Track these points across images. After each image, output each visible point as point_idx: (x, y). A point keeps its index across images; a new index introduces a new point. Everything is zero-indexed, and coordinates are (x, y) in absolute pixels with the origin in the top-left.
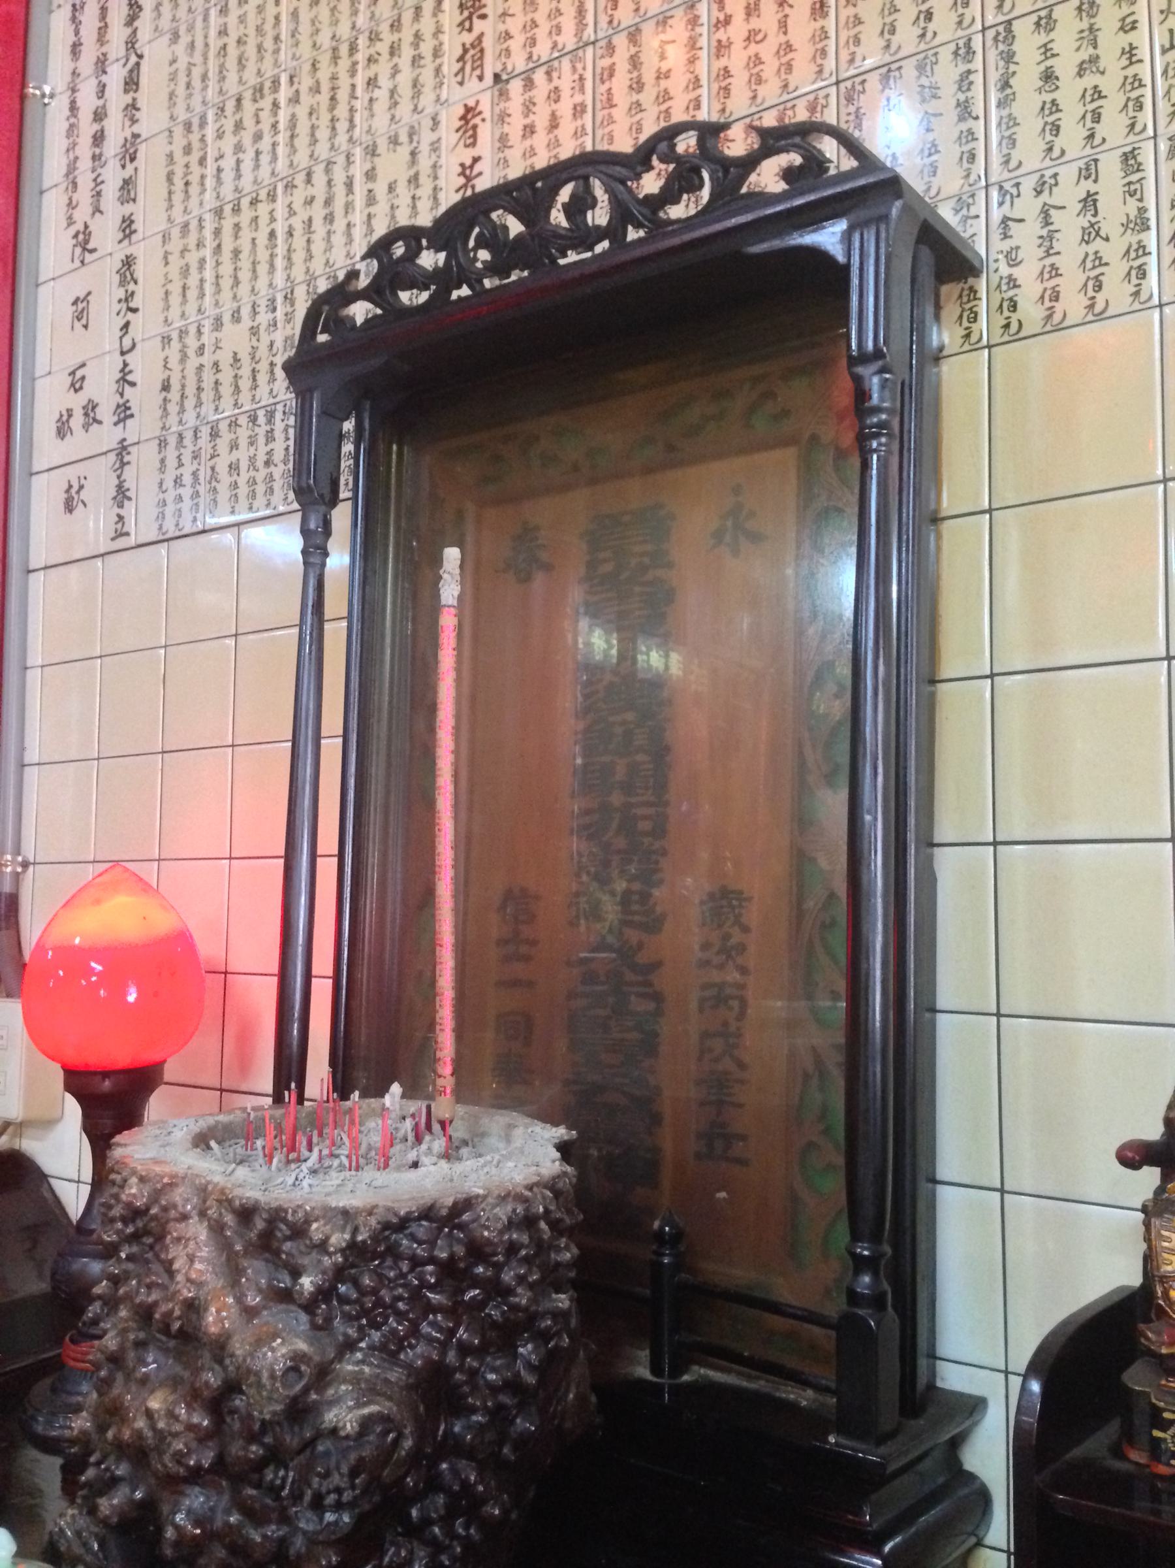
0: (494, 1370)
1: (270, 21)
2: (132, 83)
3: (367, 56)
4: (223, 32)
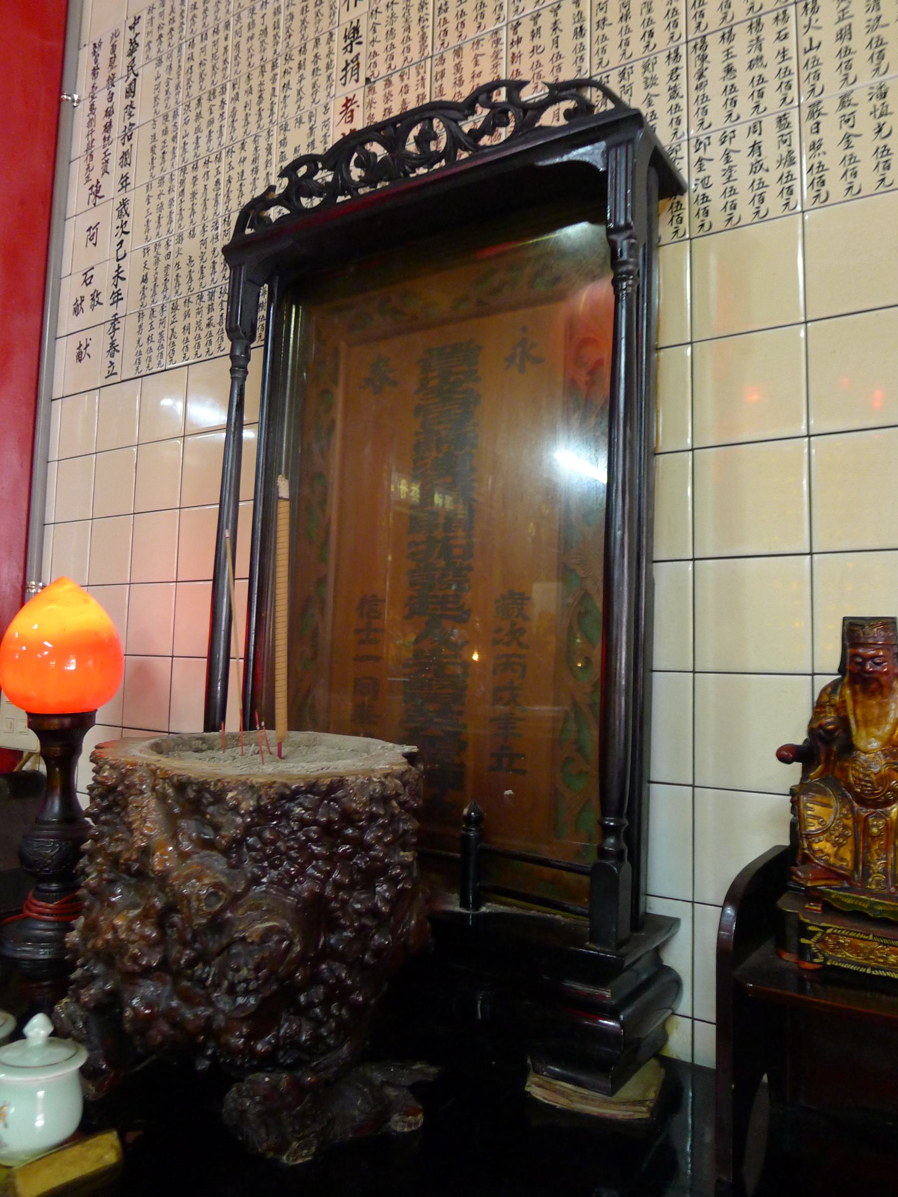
0: (358, 902)
1: (222, 50)
2: (130, 92)
3: (283, 70)
4: (191, 58)
